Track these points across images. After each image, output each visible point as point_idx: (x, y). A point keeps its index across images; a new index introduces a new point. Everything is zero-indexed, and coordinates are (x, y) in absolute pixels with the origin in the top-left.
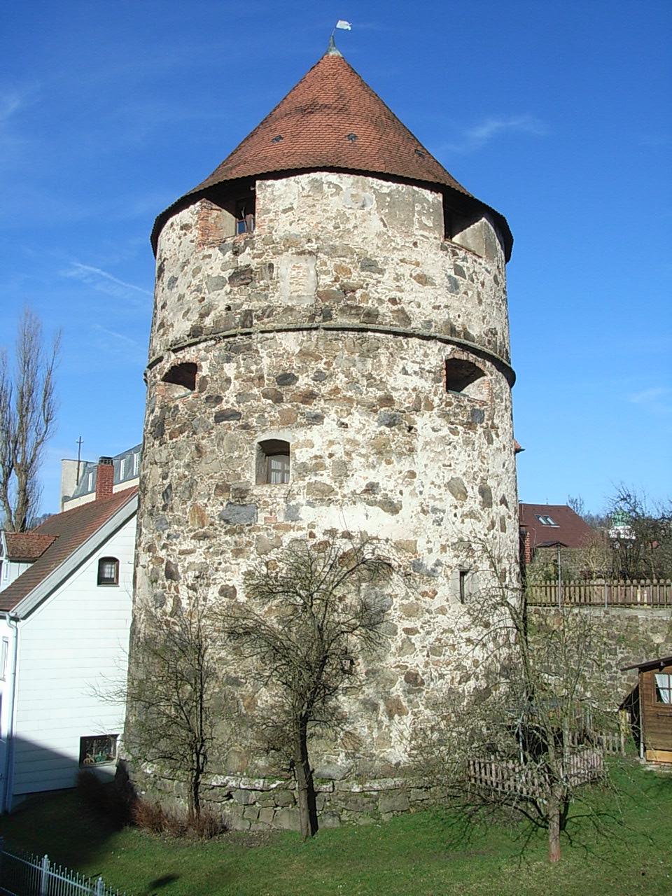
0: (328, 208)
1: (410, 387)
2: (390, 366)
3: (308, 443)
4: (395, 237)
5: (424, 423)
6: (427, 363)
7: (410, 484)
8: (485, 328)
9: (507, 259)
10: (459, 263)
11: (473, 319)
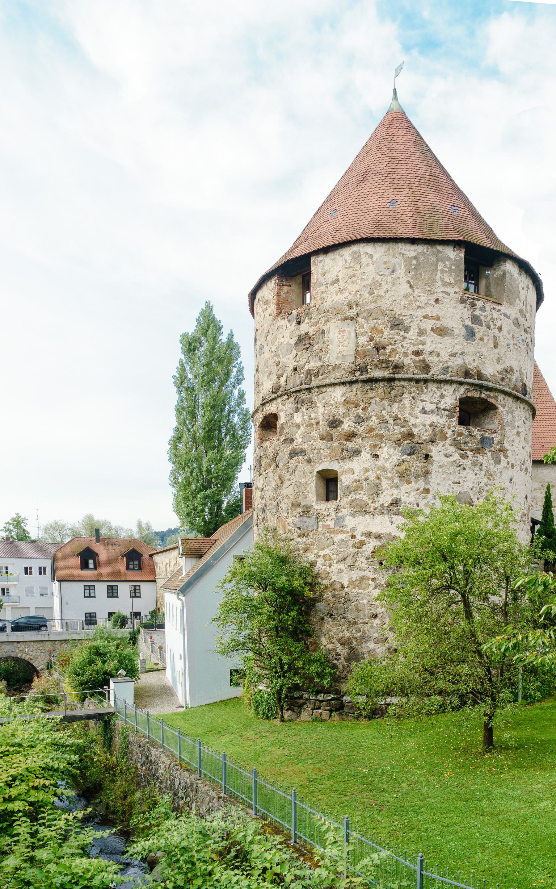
0: (364, 277)
1: (428, 422)
6: (442, 402)
7: (424, 498)
8: (500, 367)
10: (478, 313)
11: (487, 362)
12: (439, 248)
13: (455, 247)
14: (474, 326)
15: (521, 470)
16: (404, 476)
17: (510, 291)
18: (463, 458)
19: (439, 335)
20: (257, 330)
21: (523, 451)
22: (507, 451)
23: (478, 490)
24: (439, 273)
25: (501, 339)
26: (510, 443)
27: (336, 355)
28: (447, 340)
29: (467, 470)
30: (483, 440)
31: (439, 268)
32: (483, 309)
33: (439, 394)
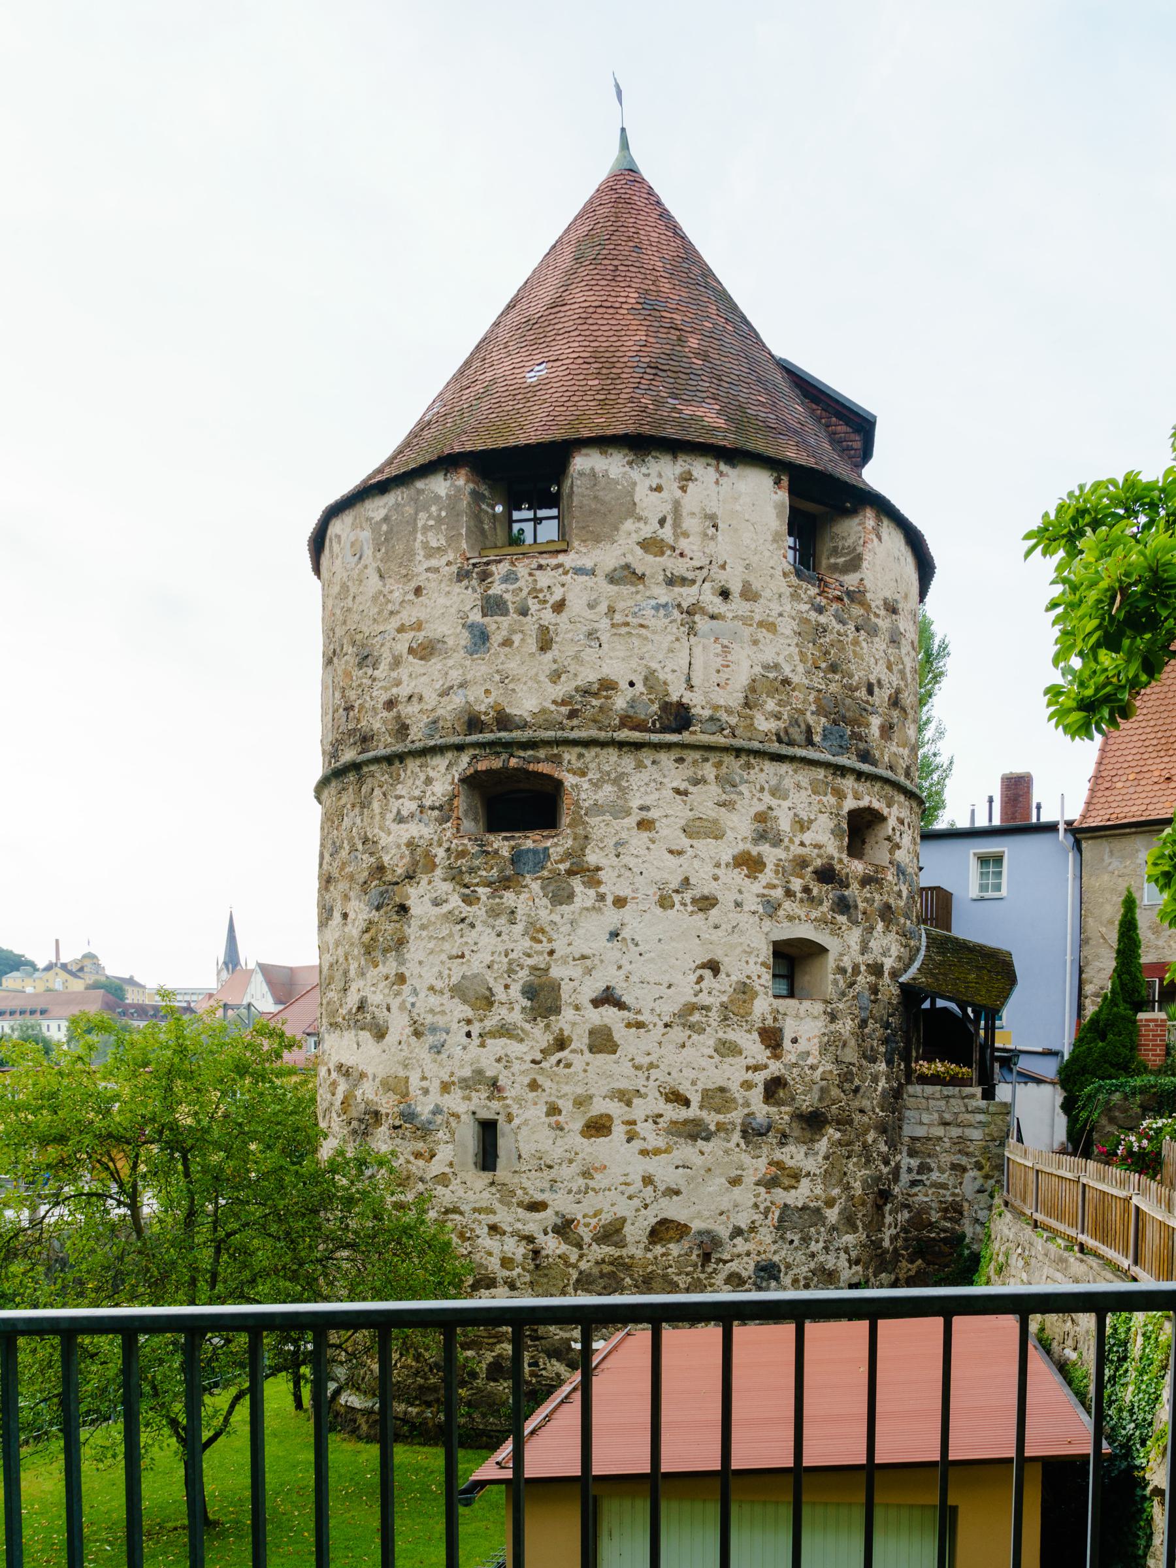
7: (398, 994)
10: (497, 589)
12: (420, 484)
14: (487, 619)
18: (470, 904)
19: (421, 659)
23: (505, 967)
28: (435, 664)
31: (420, 524)
33: (423, 777)
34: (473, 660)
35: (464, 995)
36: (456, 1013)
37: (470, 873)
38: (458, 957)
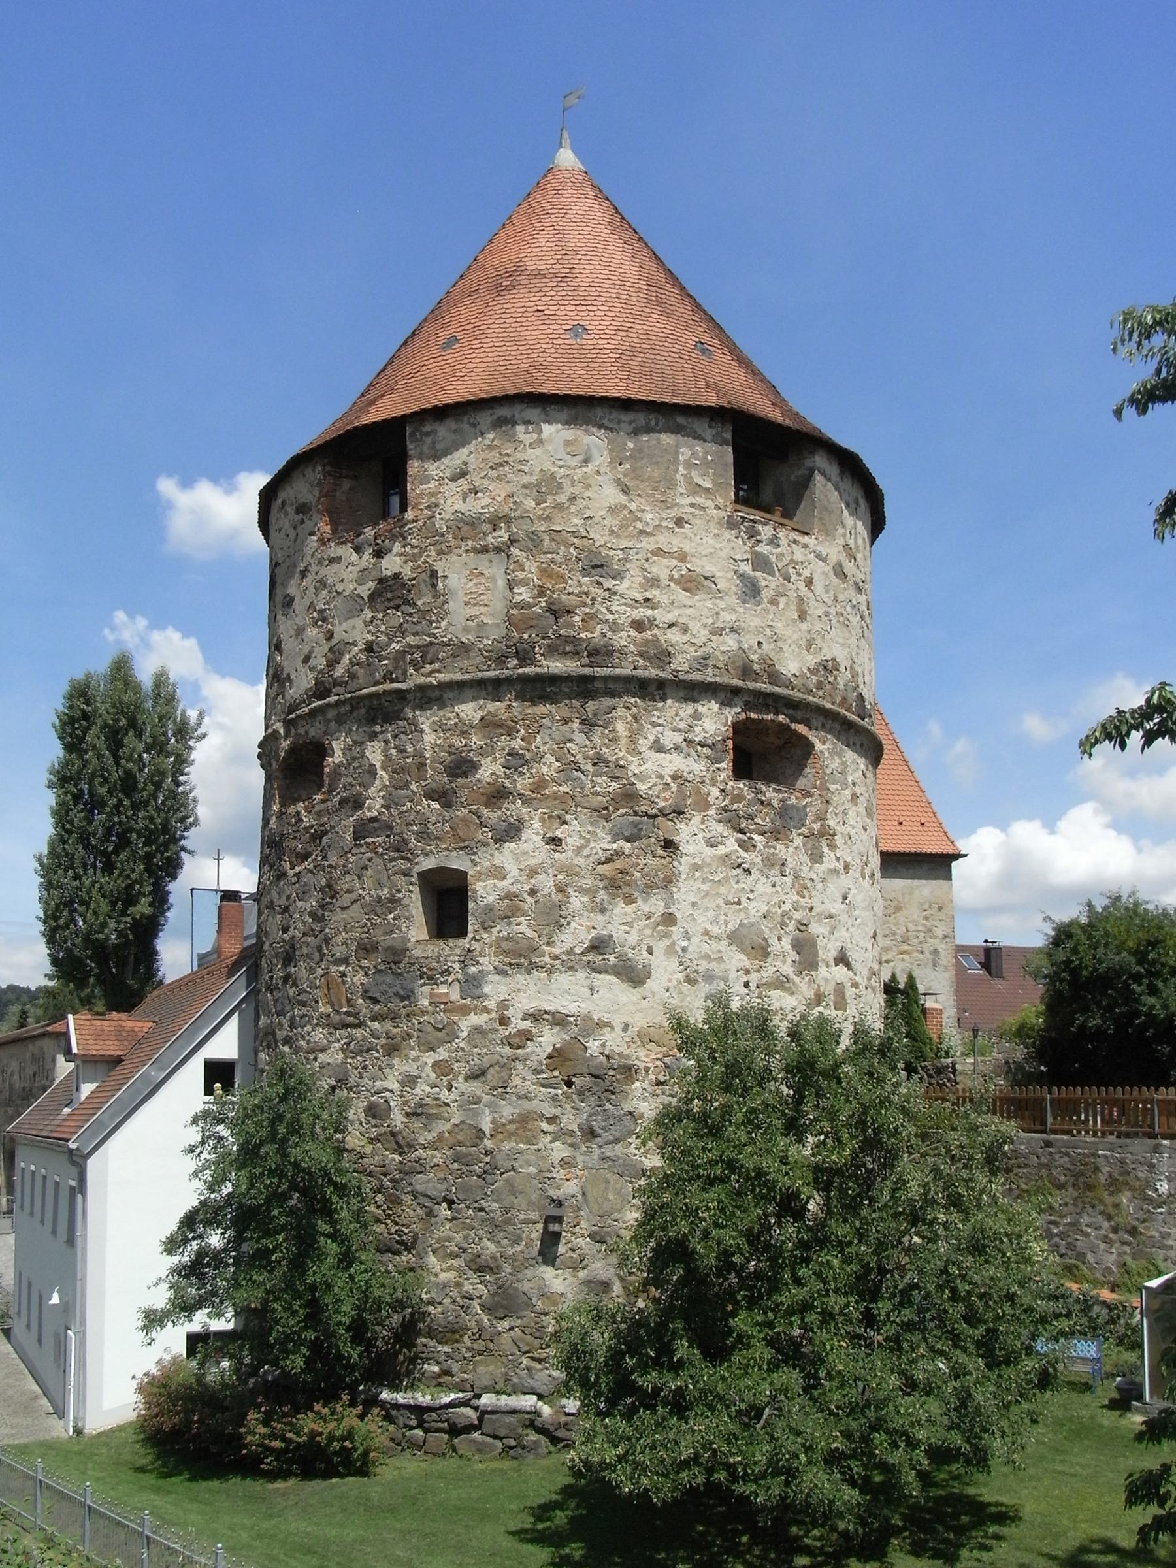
0: (526, 469)
1: (668, 771)
2: (632, 738)
3: (499, 873)
4: (643, 511)
5: (690, 834)
6: (697, 729)
7: (667, 935)
8: (811, 660)
9: (877, 526)
10: (764, 549)
11: (785, 648)
13: (712, 420)
14: (758, 574)
15: (864, 878)
16: (618, 886)
17: (826, 509)
18: (746, 850)
20: (277, 564)
21: (864, 836)
22: (834, 835)
24: (681, 468)
25: (813, 603)
26: (840, 818)
27: (463, 622)
29: (755, 874)
30: (784, 812)
32: (774, 541)
34: (746, 609)
35: (741, 943)
36: (734, 961)
37: (747, 819)
38: (734, 903)
